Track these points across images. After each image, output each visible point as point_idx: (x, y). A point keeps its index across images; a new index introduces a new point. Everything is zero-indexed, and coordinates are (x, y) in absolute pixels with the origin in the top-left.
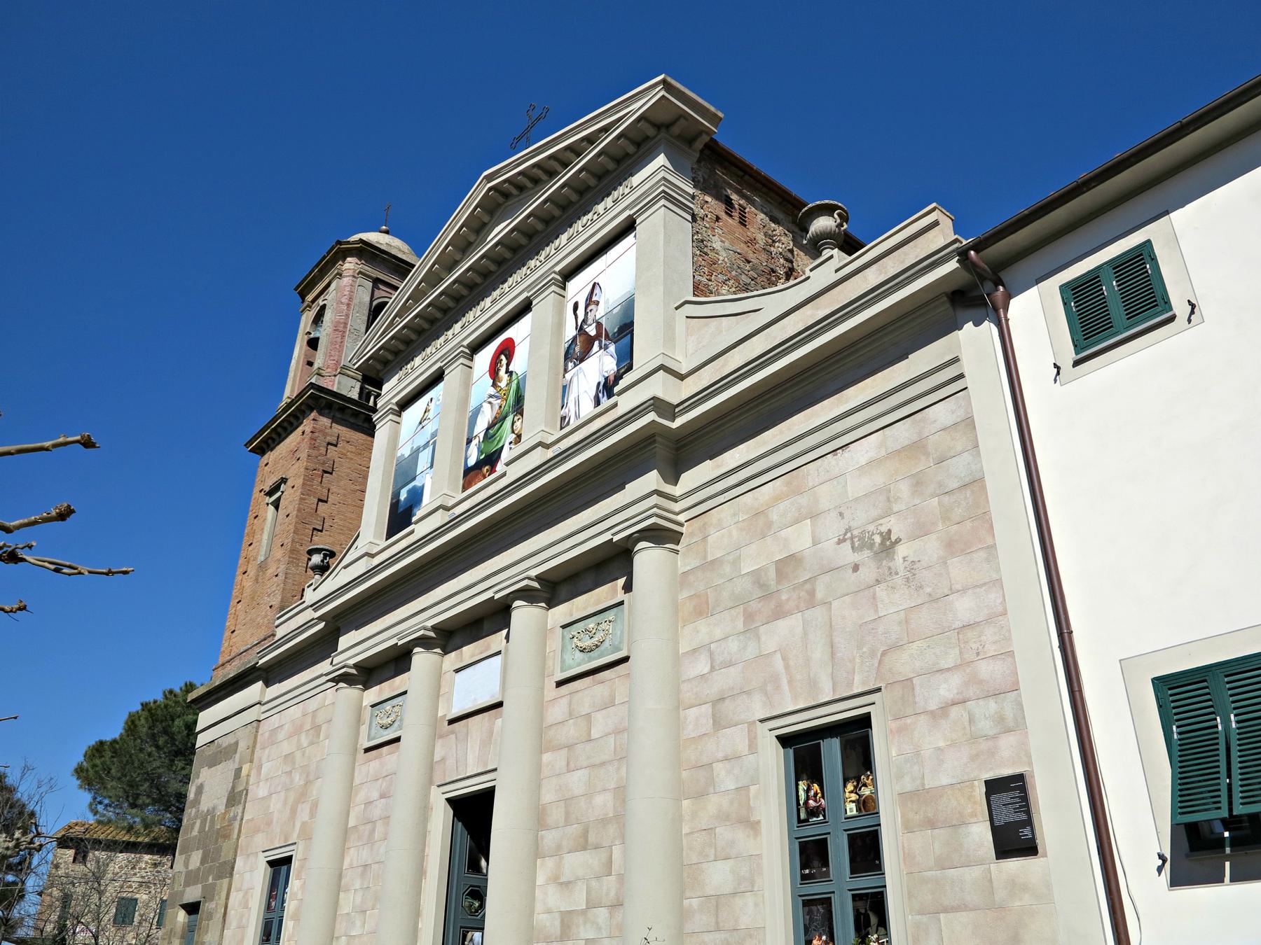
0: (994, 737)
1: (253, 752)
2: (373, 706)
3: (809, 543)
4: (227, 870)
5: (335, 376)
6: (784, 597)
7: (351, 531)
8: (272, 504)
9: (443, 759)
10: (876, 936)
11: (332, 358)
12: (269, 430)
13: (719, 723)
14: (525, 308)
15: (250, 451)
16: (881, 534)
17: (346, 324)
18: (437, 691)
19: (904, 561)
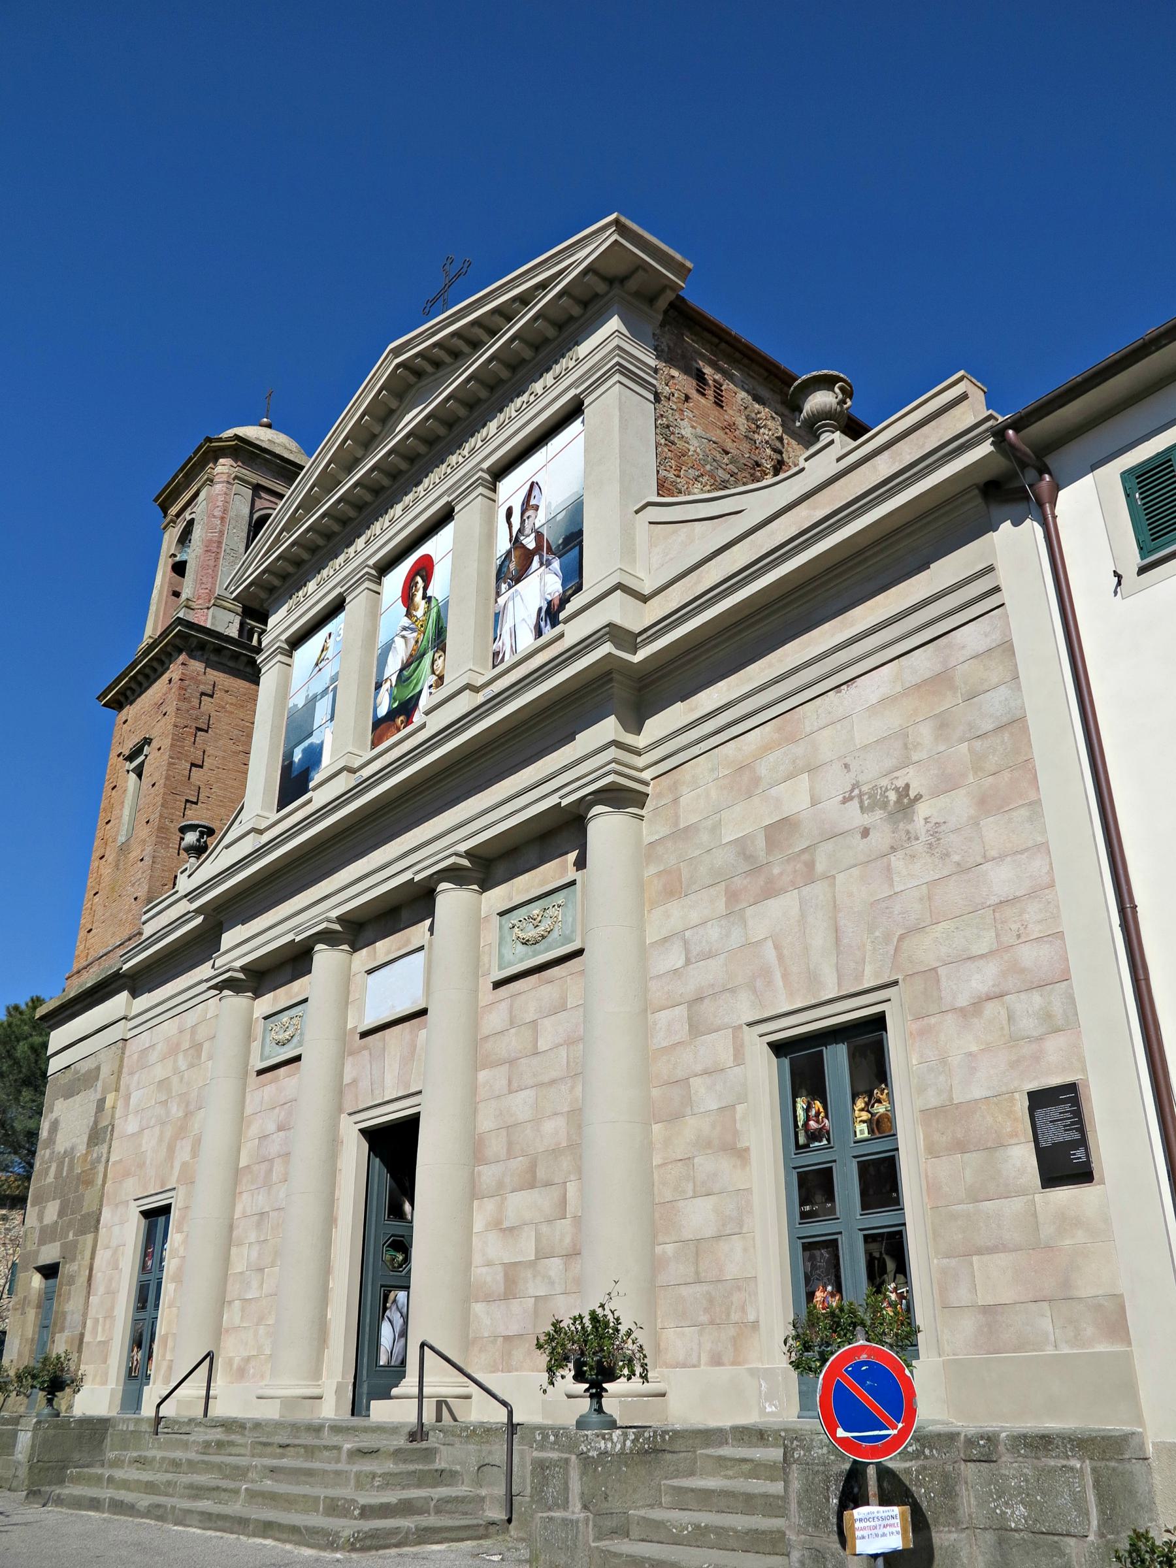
0: (1040, 1039)
1: (119, 1078)
2: (266, 1018)
4: (92, 1223)
6: (776, 871)
7: (232, 802)
9: (355, 1082)
11: (203, 586)
12: (127, 679)
13: (696, 1029)
15: (104, 705)
16: (897, 789)
17: (220, 543)
18: (345, 999)
19: (926, 822)
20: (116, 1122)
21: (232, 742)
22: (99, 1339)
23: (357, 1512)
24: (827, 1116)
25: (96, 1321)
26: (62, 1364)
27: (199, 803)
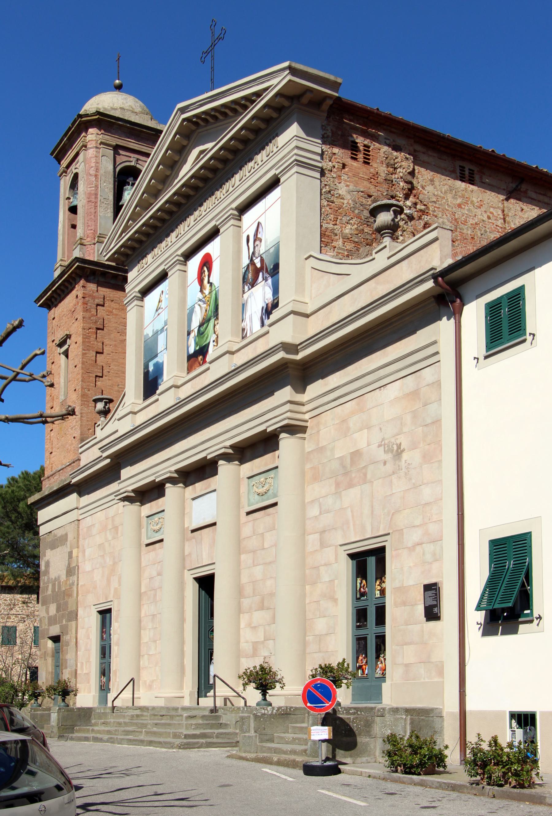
0: (431, 563)
1: (78, 541)
2: (147, 517)
3: (365, 445)
4: (74, 616)
5: (94, 244)
6: (353, 475)
8: (63, 353)
9: (190, 554)
10: (383, 655)
11: (90, 228)
12: (51, 292)
13: (323, 544)
14: (214, 233)
15: (40, 306)
16: (397, 444)
17: (96, 195)
18: (182, 513)
19: (405, 463)
20: (80, 564)
21: (119, 334)
22: (84, 672)
23: (183, 737)
24: (367, 587)
25: (82, 663)
26: (67, 684)
27: (104, 377)
